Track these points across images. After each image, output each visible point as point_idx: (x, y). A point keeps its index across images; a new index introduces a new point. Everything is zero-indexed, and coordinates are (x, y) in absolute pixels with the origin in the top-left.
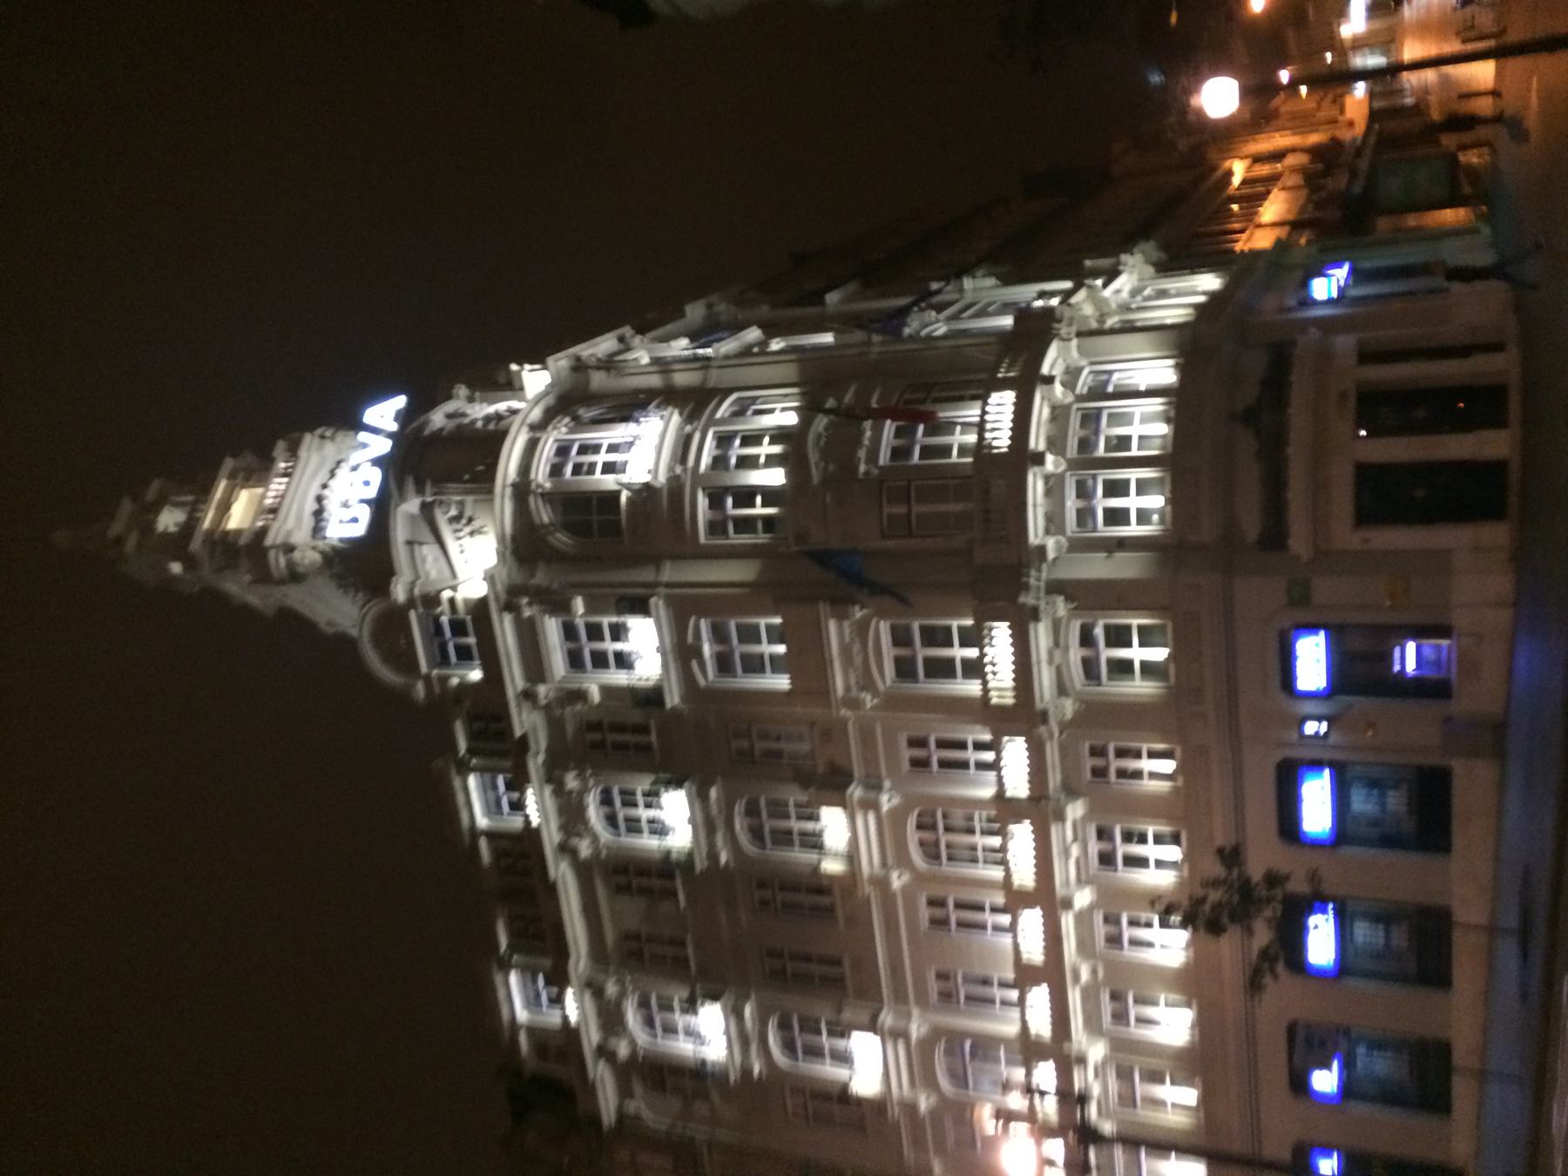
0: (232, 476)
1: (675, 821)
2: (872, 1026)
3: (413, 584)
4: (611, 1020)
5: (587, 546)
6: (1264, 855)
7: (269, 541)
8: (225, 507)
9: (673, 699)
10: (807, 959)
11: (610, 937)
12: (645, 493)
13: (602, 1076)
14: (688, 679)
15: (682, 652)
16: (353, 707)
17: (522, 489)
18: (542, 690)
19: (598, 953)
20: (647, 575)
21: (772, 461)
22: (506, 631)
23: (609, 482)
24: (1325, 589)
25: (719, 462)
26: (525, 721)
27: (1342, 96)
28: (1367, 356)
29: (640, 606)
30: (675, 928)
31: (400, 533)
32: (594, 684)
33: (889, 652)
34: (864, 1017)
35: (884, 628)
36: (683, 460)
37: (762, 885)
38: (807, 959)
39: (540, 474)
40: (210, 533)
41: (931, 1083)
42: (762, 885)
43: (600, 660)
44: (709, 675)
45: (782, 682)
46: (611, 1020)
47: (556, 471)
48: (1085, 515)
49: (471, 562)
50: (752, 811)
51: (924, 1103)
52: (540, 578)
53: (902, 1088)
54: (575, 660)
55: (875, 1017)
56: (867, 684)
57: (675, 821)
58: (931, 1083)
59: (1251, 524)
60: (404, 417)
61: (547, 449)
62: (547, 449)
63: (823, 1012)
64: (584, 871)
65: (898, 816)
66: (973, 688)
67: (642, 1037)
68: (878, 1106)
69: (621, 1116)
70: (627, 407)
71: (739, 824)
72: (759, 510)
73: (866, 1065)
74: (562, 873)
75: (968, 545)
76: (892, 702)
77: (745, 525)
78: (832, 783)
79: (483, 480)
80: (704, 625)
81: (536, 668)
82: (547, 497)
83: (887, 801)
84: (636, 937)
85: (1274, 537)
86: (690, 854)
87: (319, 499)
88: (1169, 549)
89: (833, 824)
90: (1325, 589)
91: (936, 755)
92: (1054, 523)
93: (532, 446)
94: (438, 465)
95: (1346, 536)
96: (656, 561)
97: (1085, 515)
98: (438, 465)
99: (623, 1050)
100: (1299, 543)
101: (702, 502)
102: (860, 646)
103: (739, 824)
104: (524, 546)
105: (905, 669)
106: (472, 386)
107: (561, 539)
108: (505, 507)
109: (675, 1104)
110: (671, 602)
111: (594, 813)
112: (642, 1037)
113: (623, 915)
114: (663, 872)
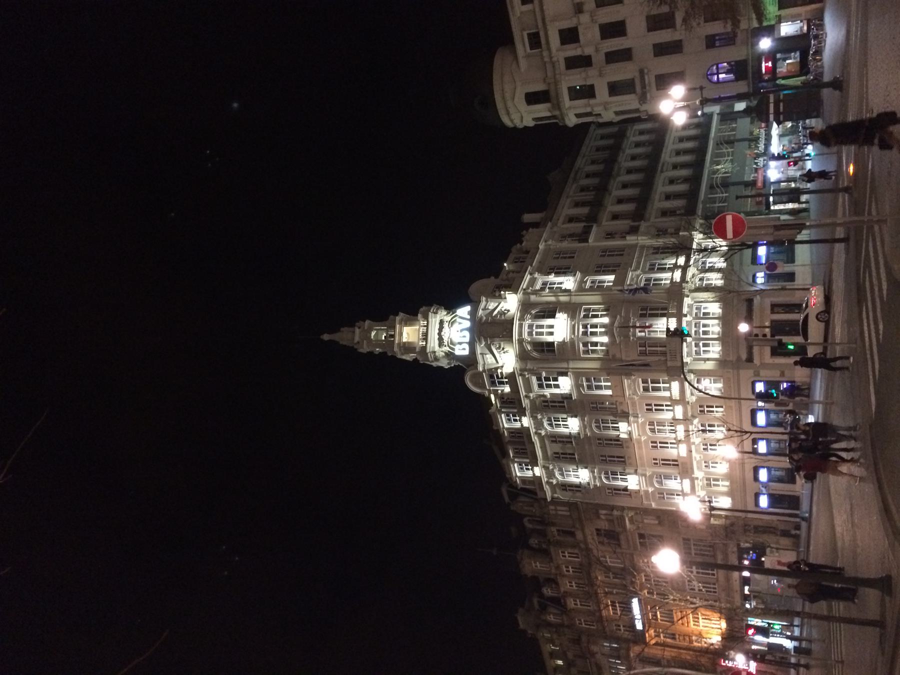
0: (400, 323)
1: (573, 425)
2: (636, 472)
3: (484, 364)
4: (551, 475)
5: (543, 356)
6: (747, 426)
7: (428, 351)
8: (401, 334)
9: (574, 397)
10: (614, 457)
11: (549, 453)
12: (563, 344)
13: (547, 488)
14: (579, 392)
15: (578, 386)
16: (450, 389)
17: (521, 341)
18: (531, 395)
19: (546, 457)
20: (564, 365)
21: (602, 334)
22: (520, 381)
23: (550, 339)
24: (763, 373)
25: (585, 333)
26: (526, 403)
27: (721, 613)
28: (775, 307)
29: (565, 374)
30: (568, 451)
31: (479, 351)
32: (547, 392)
33: (641, 385)
34: (633, 471)
35: (640, 380)
36: (574, 333)
37: (599, 439)
38: (614, 457)
39: (525, 336)
40: (399, 344)
41: (652, 485)
42: (599, 439)
43: (549, 386)
44: (586, 391)
45: (609, 392)
46: (551, 475)
47: (530, 334)
48: (698, 353)
49: (507, 360)
50: (597, 422)
51: (650, 490)
52: (529, 366)
53: (644, 487)
54: (541, 386)
55: (636, 471)
56: (635, 393)
57: (573, 425)
58: (652, 485)
59: (744, 356)
60: (471, 313)
61: (526, 329)
62: (526, 329)
63: (619, 469)
64: (542, 439)
65: (643, 424)
66: (667, 394)
67: (560, 478)
68: (637, 492)
69: (553, 498)
70: (549, 312)
71: (593, 425)
72: (599, 348)
73: (632, 482)
74: (535, 439)
75: (666, 358)
76: (642, 397)
77: (593, 351)
78: (625, 416)
79: (509, 337)
80: (584, 379)
81: (529, 389)
82: (529, 343)
83: (640, 420)
84: (557, 453)
85: (750, 359)
86: (579, 434)
87: (439, 334)
88: (722, 363)
89: (623, 426)
90: (763, 373)
91: (654, 408)
92: (689, 354)
93: (521, 326)
94: (491, 330)
95: (768, 359)
96: (567, 361)
97: (698, 353)
98: (491, 330)
99: (554, 482)
100: (757, 361)
101: (581, 345)
102: (633, 387)
103: (593, 425)
104: (523, 356)
105: (646, 389)
106: (487, 297)
107: (535, 354)
108: (516, 344)
109: (570, 493)
110: (574, 373)
111: (546, 424)
112: (560, 478)
113: (551, 448)
114: (568, 439)
